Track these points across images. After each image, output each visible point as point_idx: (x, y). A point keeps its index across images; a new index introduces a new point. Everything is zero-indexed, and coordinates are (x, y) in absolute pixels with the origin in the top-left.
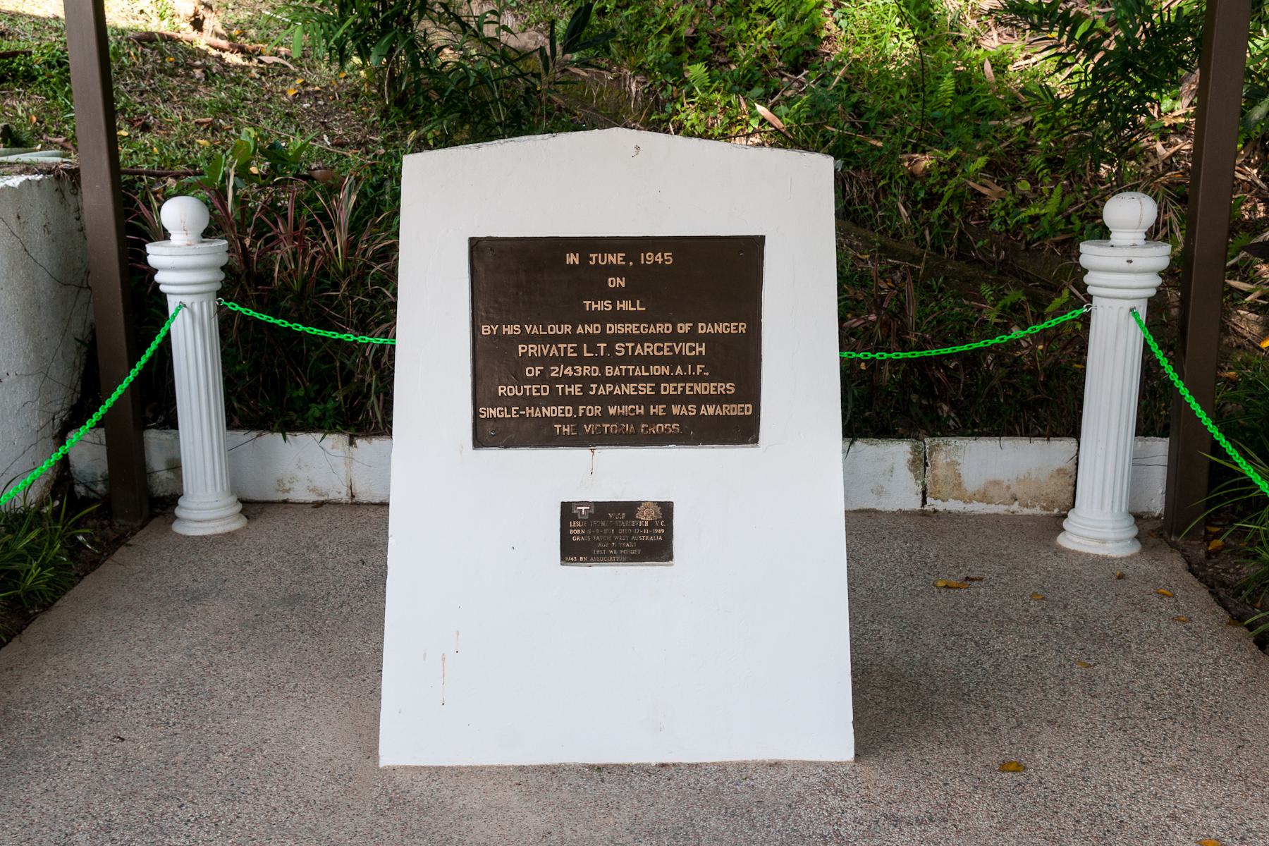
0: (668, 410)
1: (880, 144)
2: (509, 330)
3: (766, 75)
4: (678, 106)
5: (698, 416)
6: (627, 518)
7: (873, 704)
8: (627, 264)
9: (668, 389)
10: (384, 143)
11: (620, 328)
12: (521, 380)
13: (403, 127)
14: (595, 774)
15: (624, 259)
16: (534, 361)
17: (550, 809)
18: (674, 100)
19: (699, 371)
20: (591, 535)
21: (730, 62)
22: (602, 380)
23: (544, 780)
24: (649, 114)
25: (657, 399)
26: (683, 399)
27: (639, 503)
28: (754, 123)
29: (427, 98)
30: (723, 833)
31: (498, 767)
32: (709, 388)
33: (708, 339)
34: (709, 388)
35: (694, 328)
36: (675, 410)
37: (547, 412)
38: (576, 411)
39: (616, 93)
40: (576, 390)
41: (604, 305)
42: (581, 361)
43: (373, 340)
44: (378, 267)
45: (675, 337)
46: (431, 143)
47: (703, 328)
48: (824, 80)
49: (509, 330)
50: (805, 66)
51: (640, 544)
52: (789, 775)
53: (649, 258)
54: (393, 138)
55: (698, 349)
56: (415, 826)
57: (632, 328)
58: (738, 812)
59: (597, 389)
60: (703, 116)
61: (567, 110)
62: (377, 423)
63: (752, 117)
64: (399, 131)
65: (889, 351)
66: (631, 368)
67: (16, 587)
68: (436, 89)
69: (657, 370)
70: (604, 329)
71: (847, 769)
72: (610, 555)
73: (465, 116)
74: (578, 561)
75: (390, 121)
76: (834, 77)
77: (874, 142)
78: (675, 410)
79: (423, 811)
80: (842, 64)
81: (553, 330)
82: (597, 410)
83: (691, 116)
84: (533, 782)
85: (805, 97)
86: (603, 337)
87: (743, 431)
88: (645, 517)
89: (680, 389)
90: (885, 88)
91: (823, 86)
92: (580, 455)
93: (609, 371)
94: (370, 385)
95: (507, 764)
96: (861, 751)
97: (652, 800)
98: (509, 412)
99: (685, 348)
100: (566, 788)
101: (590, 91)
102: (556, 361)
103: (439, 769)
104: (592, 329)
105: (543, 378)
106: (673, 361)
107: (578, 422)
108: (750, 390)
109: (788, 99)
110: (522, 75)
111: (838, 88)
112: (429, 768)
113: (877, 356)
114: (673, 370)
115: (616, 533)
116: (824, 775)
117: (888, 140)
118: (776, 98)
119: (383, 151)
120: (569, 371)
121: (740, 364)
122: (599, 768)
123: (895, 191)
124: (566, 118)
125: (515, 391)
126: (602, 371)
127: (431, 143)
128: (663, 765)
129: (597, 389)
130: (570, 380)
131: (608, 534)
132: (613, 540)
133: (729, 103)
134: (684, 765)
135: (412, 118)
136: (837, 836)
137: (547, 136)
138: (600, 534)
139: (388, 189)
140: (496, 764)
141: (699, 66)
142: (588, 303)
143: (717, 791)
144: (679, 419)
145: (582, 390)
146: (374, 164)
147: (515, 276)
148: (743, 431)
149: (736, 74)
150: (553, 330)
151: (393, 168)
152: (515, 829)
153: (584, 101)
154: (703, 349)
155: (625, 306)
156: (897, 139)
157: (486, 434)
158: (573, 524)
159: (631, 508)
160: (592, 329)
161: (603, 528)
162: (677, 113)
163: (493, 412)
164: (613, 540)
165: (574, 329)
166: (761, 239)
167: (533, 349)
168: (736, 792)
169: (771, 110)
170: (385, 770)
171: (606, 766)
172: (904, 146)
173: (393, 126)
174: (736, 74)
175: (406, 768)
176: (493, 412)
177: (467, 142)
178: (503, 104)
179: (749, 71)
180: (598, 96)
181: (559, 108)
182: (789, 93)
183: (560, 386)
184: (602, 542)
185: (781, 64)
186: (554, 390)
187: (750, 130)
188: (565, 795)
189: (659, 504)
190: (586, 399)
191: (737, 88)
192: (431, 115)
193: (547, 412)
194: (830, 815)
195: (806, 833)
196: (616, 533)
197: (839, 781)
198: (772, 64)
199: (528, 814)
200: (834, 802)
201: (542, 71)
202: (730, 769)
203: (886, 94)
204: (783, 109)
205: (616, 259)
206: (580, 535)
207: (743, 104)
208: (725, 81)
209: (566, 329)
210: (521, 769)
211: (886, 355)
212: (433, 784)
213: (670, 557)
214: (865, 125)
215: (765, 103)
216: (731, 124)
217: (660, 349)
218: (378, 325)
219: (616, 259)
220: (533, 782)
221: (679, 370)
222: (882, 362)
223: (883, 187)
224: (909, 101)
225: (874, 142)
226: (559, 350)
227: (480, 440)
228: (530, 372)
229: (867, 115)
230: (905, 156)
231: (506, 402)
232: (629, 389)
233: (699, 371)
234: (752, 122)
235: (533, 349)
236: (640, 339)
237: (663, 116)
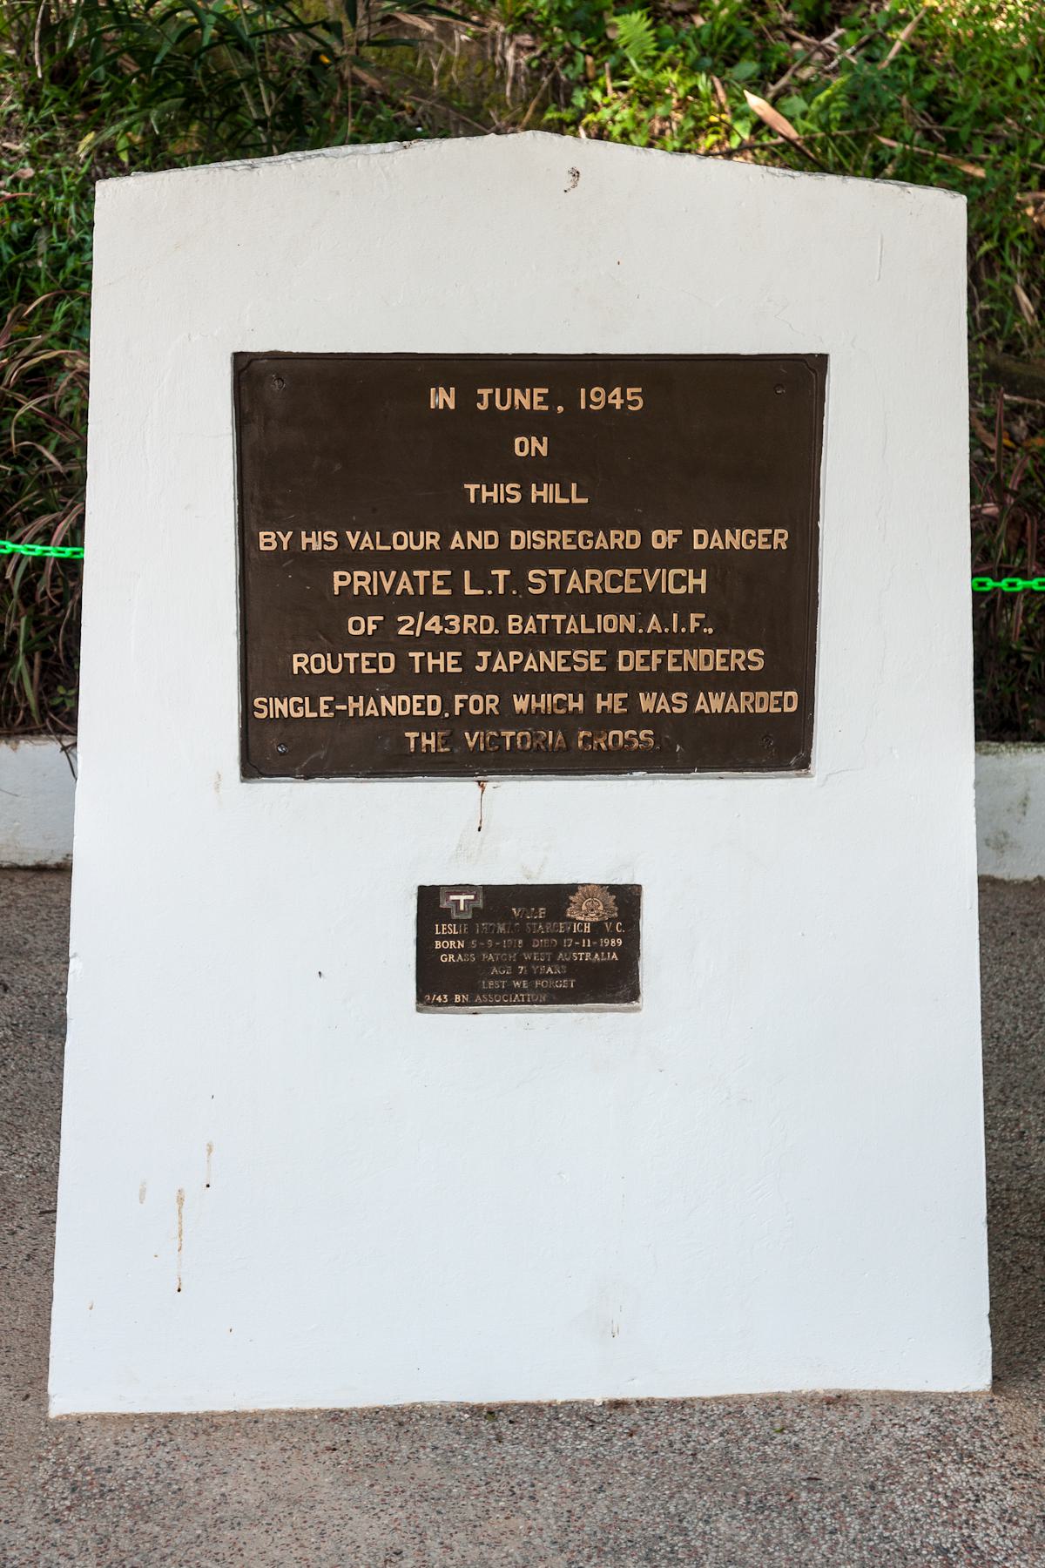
0: (631, 703)
1: (980, 173)
2: (314, 541)
3: (761, 36)
4: (597, 95)
5: (694, 717)
6: (549, 917)
7: (1017, 1271)
8: (553, 410)
9: (632, 661)
10: (31, 157)
11: (538, 539)
12: (338, 642)
13: (68, 124)
14: (484, 1425)
15: (547, 399)
16: (363, 604)
17: (398, 1501)
18: (587, 82)
19: (693, 625)
21: (694, 11)
22: (501, 643)
23: (382, 1440)
24: (541, 110)
25: (610, 680)
26: (661, 682)
27: (573, 888)
28: (742, 131)
29: (114, 69)
30: (745, 1546)
31: (290, 1413)
32: (713, 659)
33: (712, 561)
34: (713, 659)
35: (685, 541)
36: (647, 703)
37: (392, 706)
38: (448, 705)
39: (477, 67)
40: (448, 662)
41: (506, 493)
42: (459, 604)
43: (22, 549)
44: (31, 404)
45: (647, 557)
46: (124, 157)
47: (702, 540)
48: (871, 47)
49: (314, 541)
50: (836, 20)
51: (573, 969)
52: (866, 1421)
53: (596, 398)
54: (50, 146)
55: (692, 581)
56: (125, 1544)
57: (560, 539)
58: (771, 1501)
59: (491, 661)
60: (644, 115)
61: (385, 98)
62: (27, 709)
63: (739, 117)
64: (61, 133)
65: (1024, 575)
66: (559, 618)
68: (132, 51)
69: (608, 623)
70: (505, 541)
71: (978, 1408)
72: (511, 990)
73: (193, 103)
74: (451, 1002)
75: (44, 113)
76: (891, 43)
77: (970, 169)
78: (647, 703)
79: (141, 1509)
80: (906, 19)
81: (403, 541)
82: (491, 703)
83: (617, 111)
84: (360, 1444)
85: (837, 81)
86: (503, 556)
87: (781, 745)
88: (583, 914)
89: (655, 661)
90: (989, 65)
91: (870, 59)
92: (457, 793)
93: (514, 624)
94: (14, 637)
95: (307, 1406)
96: (1006, 1369)
97: (598, 1478)
98: (314, 707)
99: (666, 580)
100: (427, 1456)
101: (426, 64)
102: (410, 604)
103: (171, 1419)
104: (482, 540)
105: (384, 638)
106: (646, 603)
107: (453, 725)
108: (794, 662)
109: (805, 84)
110: (300, 27)
111: (898, 64)
112: (150, 1418)
113: (1003, 584)
114: (642, 622)
115: (527, 947)
116: (935, 1420)
117: (995, 166)
118: (783, 81)
119: (30, 172)
120: (434, 625)
121: (776, 611)
122: (492, 1413)
123: (1010, 263)
124: (385, 114)
125: (326, 665)
126: (501, 624)
127: (124, 157)
128: (618, 1405)
129: (491, 661)
130: (436, 643)
131: (510, 950)
132: (520, 960)
133: (694, 91)
134: (659, 1402)
135: (87, 108)
136: (970, 1550)
137: (390, 146)
138: (495, 949)
139: (42, 248)
140: (285, 1406)
141: (636, 17)
142: (472, 487)
143: (727, 1458)
144: (654, 720)
145: (460, 662)
146: (14, 199)
147: (319, 431)
148: (781, 745)
149: (705, 33)
150: (403, 541)
151: (50, 205)
152: (328, 1546)
153: (419, 82)
154: (702, 582)
155: (548, 493)
156: (1015, 164)
157: (267, 752)
158: (442, 929)
159: (556, 897)
160: (482, 540)
161: (499, 937)
162: (593, 107)
163: (282, 707)
164: (520, 960)
165: (446, 539)
166: (818, 364)
167: (362, 581)
168: (764, 1458)
169: (774, 103)
170: (61, 1423)
171: (504, 1407)
172: (1025, 176)
173: (48, 123)
174: (705, 33)
175: (103, 1418)
176: (282, 707)
177: (195, 159)
178: (268, 83)
179: (730, 28)
180: (442, 72)
181: (371, 95)
182: (806, 73)
183: (417, 655)
184: (499, 964)
185: (789, 16)
186: (404, 663)
187: (734, 143)
188: (426, 1471)
189: (613, 889)
190: (469, 680)
191: (708, 61)
192: (124, 103)
193: (392, 706)
194: (952, 1505)
195: (907, 1543)
196: (527, 947)
197: (964, 1434)
198: (773, 15)
199: (354, 1512)
200: (958, 1477)
201: (344, 20)
202: (749, 1410)
203: (991, 76)
204: (797, 103)
205: (529, 399)
206: (455, 952)
207: (721, 93)
208: (685, 47)
209: (430, 539)
210: (335, 1416)
211: (1021, 584)
212: (160, 1453)
213: (634, 995)
214: (952, 136)
215: (763, 93)
216: (698, 132)
217: (616, 581)
218: (29, 517)
219: (529, 399)
220: (360, 1444)
221: (654, 624)
222: (1010, 599)
223: (987, 254)
224: (1033, 91)
225: (970, 169)
226: (414, 581)
227: (255, 765)
228: (356, 625)
229: (955, 117)
230: (1028, 197)
231: (310, 686)
232: (553, 661)
233: (693, 625)
234: (738, 126)
235: (362, 581)
236: (576, 561)
237: (567, 115)
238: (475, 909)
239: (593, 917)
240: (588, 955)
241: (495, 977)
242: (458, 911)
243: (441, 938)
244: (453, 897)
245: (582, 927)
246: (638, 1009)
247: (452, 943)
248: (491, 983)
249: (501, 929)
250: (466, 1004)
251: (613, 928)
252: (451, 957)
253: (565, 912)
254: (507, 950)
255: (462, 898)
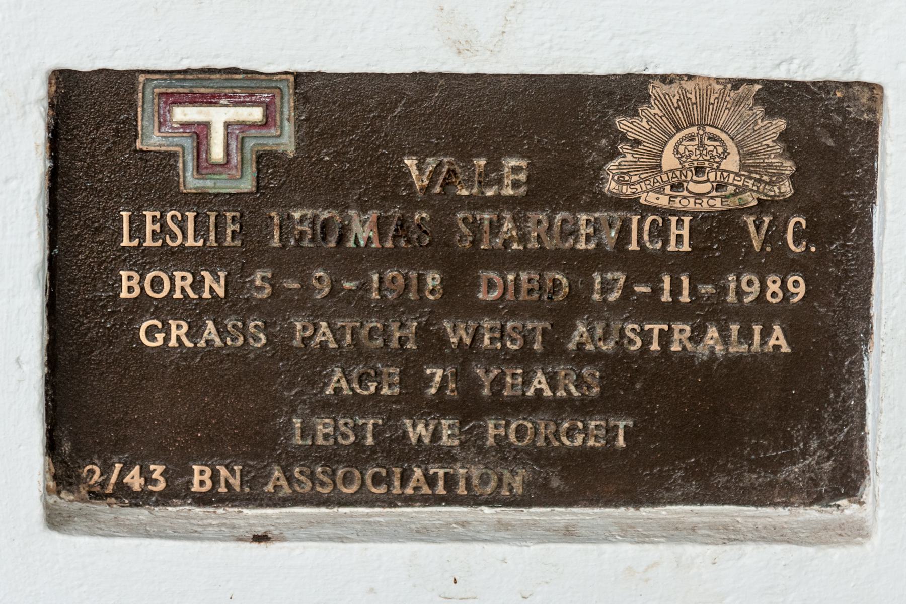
6: (542, 192)
20: (275, 310)
27: (629, 91)
51: (628, 381)
67: (561, 289)
72: (397, 453)
74: (177, 492)
131: (397, 308)
132: (433, 345)
138: (339, 303)
159: (565, 123)
161: (353, 261)
184: (357, 354)
189: (777, 96)
196: (459, 298)
206: (195, 312)
213: (845, 476)
238: (266, 160)
239: (702, 197)
240: (682, 331)
241: (339, 405)
242: (203, 165)
243: (143, 260)
244: (183, 114)
245: (661, 232)
246: (856, 532)
247: (183, 280)
248: (323, 426)
249: (363, 230)
250: (231, 499)
251: (775, 236)
252: (179, 330)
253: (597, 177)
254: (385, 309)
255: (218, 117)
